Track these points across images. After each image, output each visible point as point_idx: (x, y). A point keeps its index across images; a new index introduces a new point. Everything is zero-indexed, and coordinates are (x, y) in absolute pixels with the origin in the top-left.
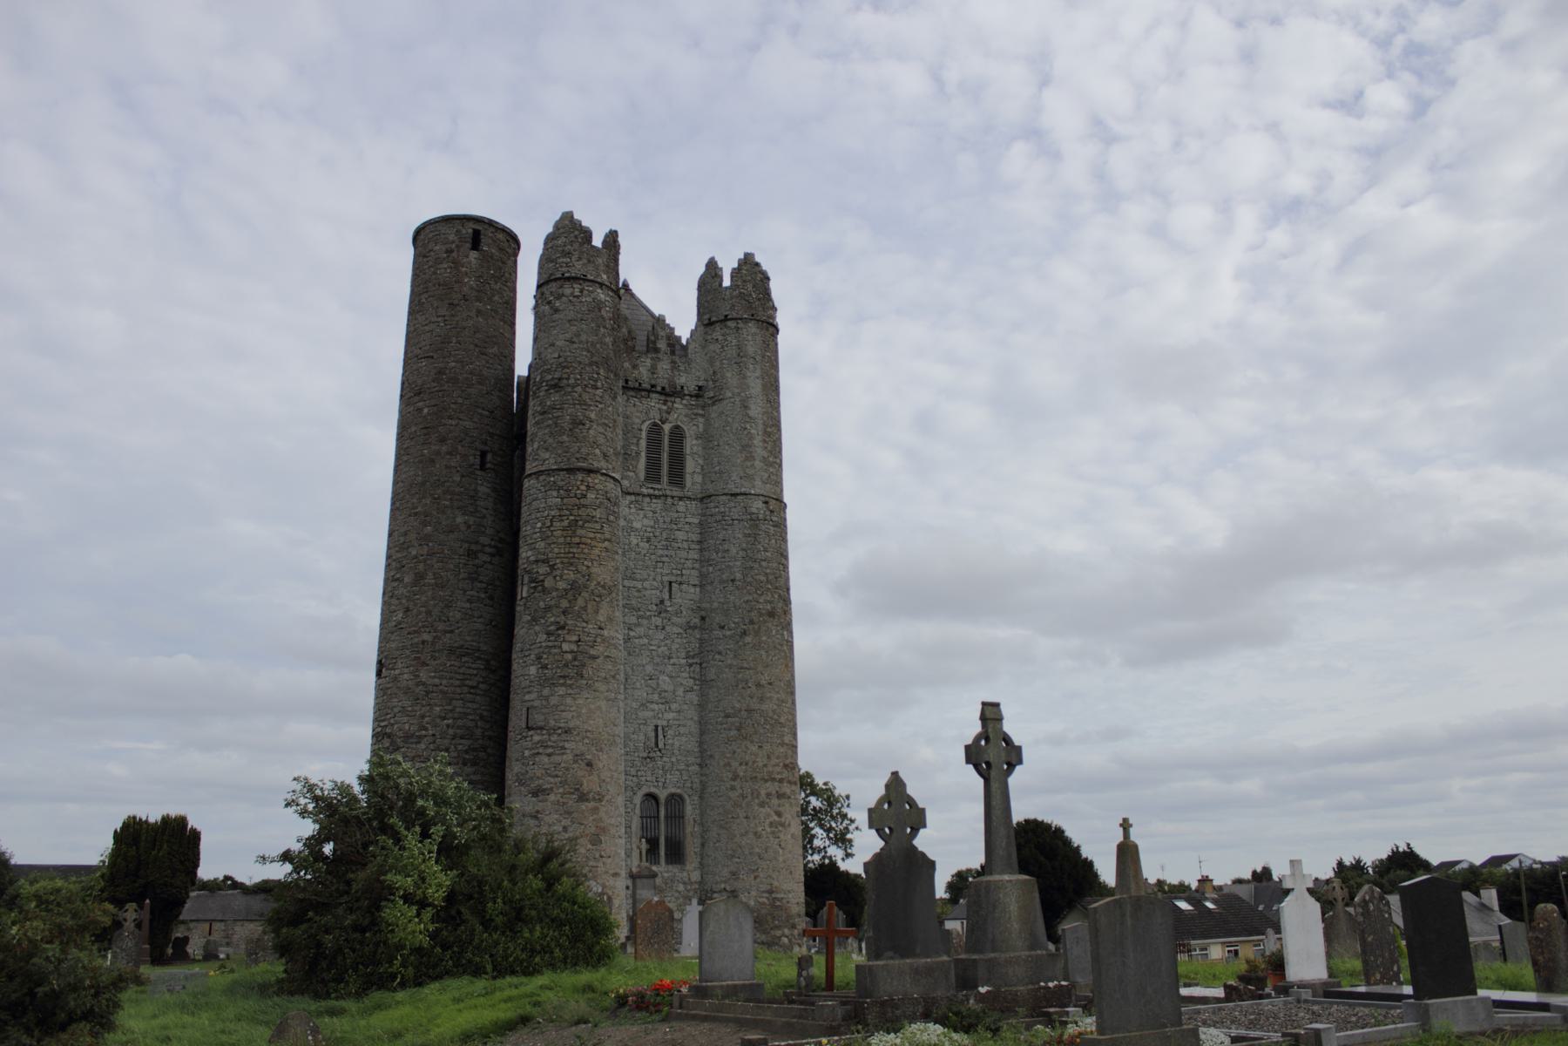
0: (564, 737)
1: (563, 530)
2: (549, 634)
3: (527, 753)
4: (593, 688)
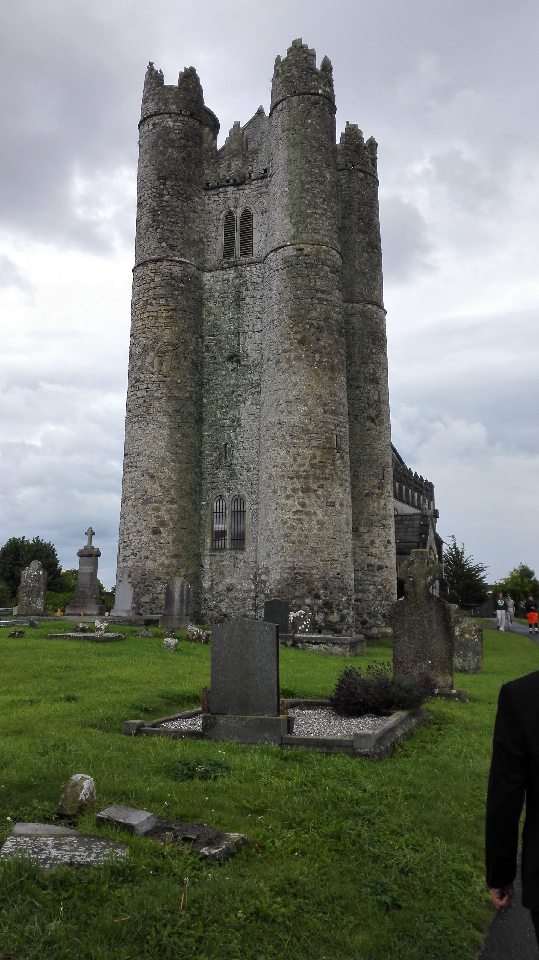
0: (137, 459)
1: (140, 310)
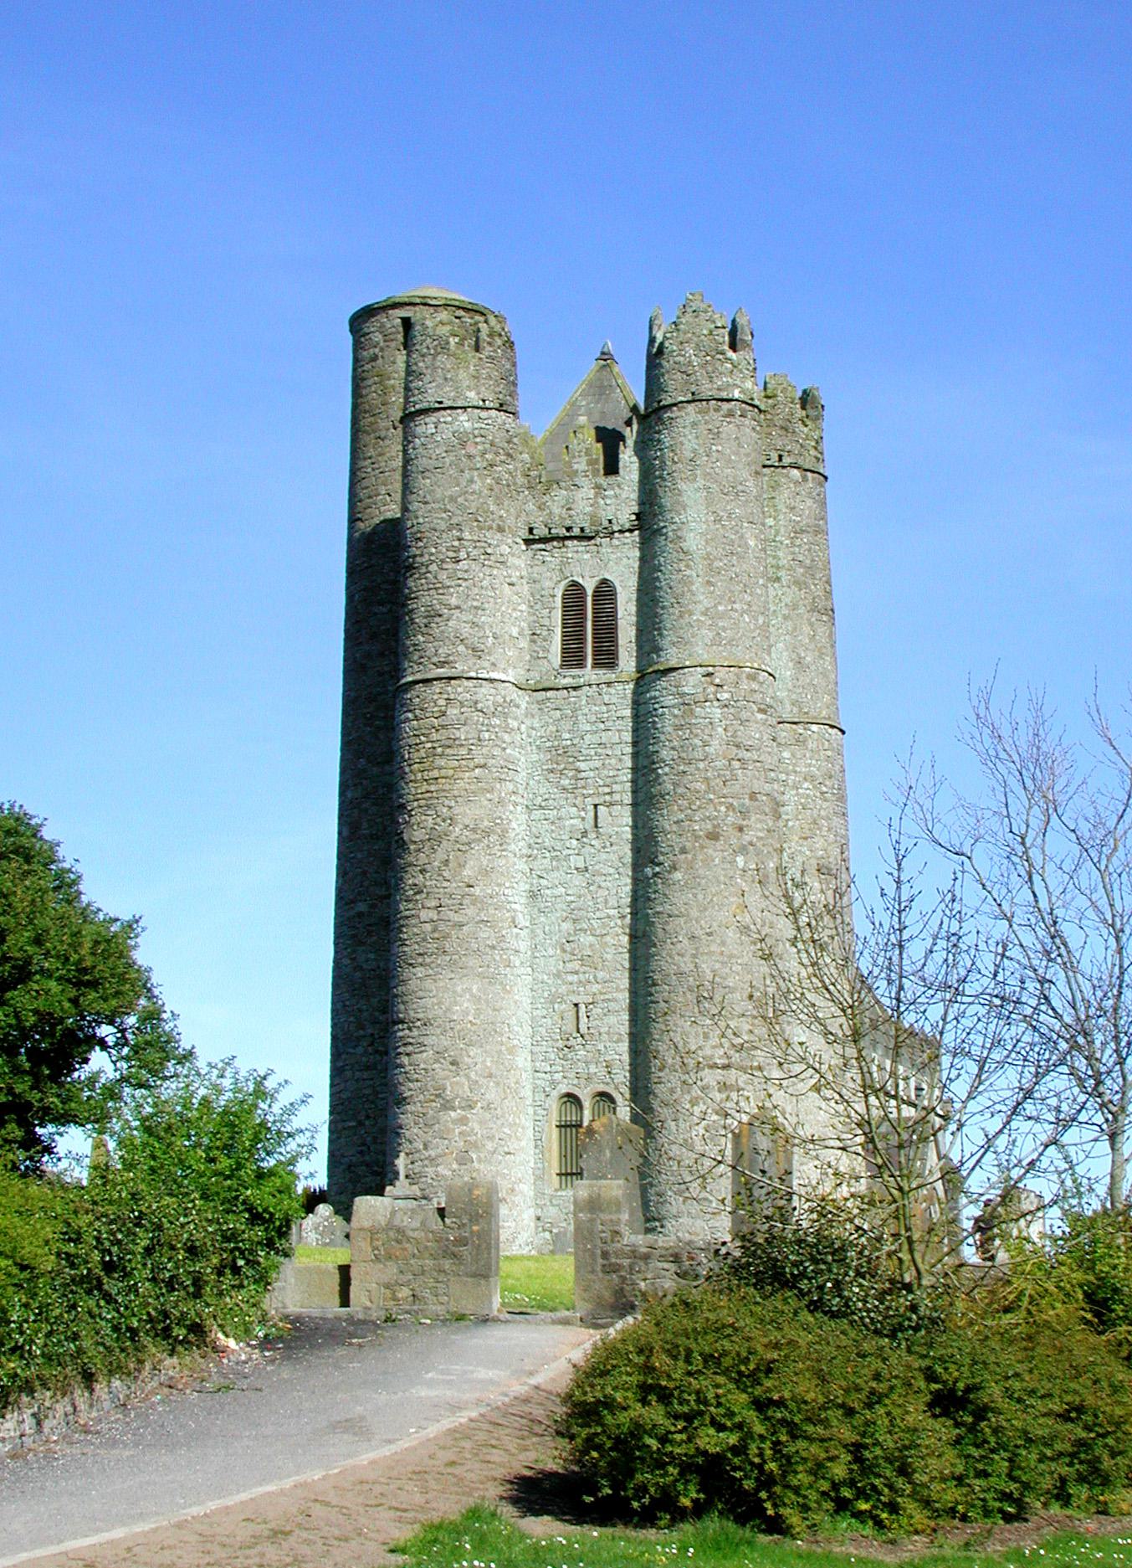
4: (460, 964)
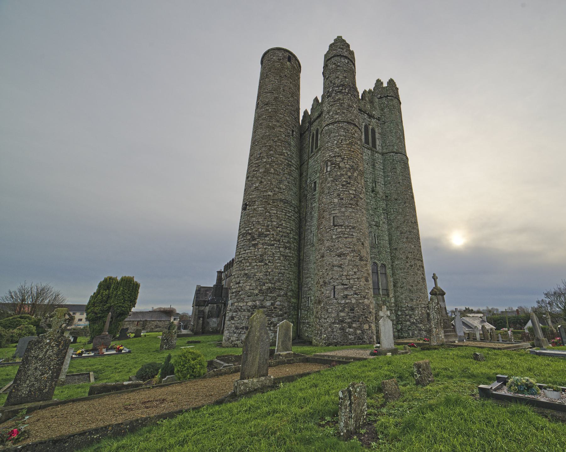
0: (352, 230)
1: (347, 145)
2: (343, 185)
3: (334, 237)
